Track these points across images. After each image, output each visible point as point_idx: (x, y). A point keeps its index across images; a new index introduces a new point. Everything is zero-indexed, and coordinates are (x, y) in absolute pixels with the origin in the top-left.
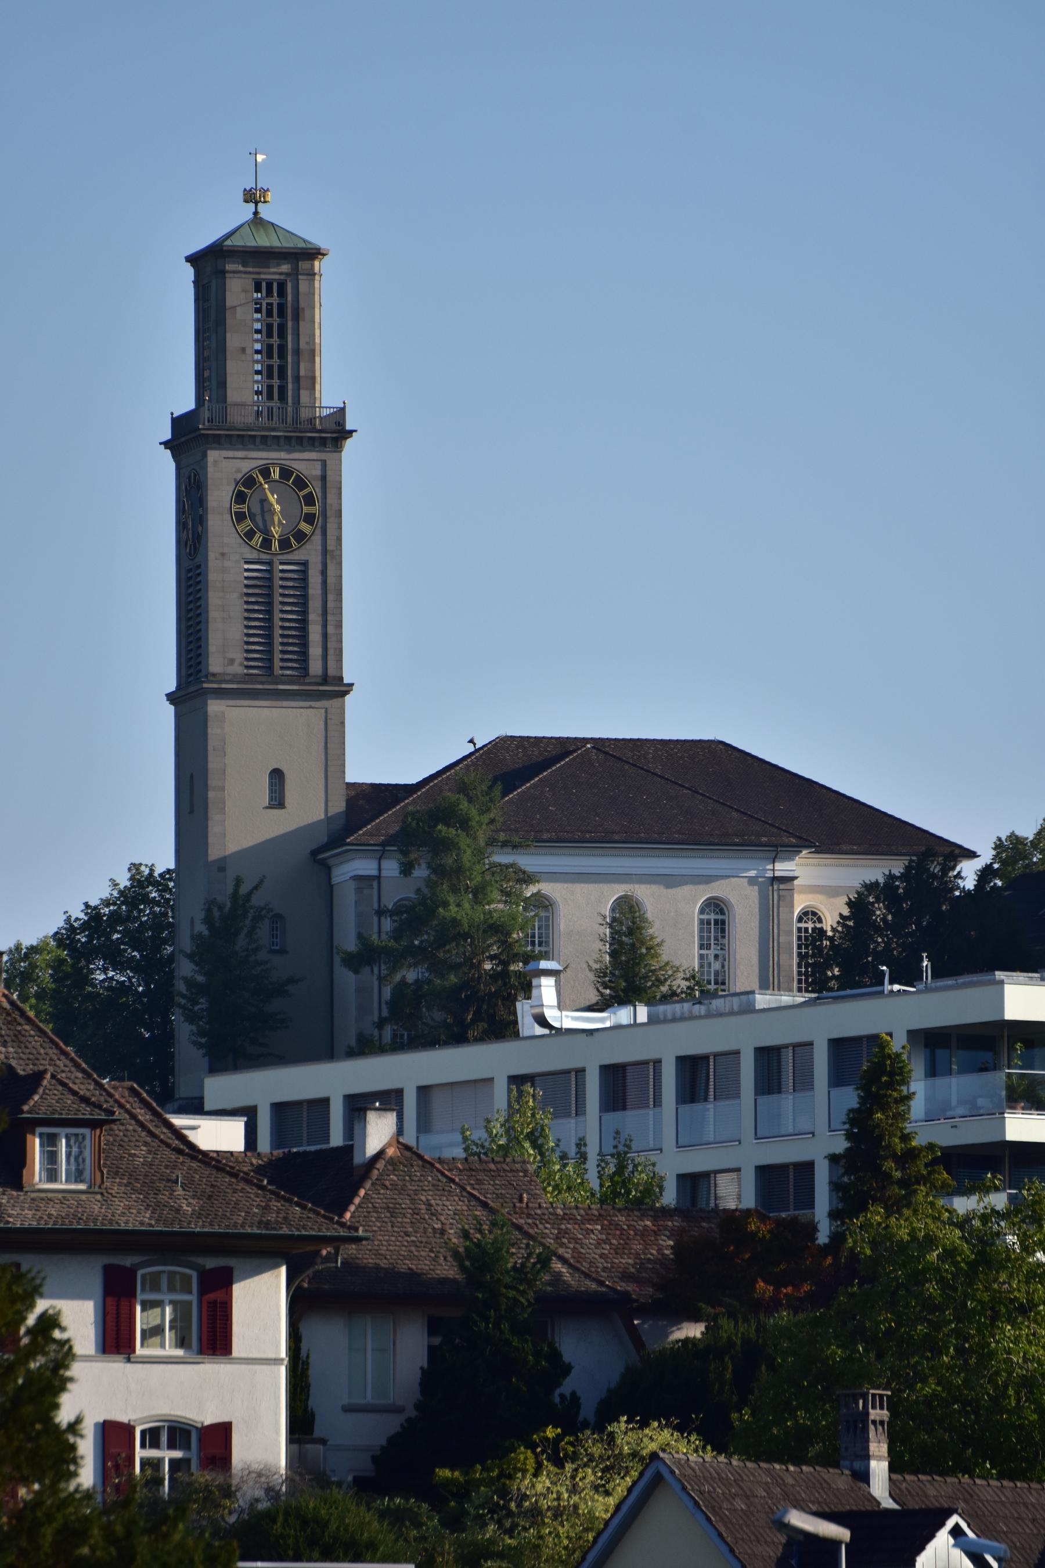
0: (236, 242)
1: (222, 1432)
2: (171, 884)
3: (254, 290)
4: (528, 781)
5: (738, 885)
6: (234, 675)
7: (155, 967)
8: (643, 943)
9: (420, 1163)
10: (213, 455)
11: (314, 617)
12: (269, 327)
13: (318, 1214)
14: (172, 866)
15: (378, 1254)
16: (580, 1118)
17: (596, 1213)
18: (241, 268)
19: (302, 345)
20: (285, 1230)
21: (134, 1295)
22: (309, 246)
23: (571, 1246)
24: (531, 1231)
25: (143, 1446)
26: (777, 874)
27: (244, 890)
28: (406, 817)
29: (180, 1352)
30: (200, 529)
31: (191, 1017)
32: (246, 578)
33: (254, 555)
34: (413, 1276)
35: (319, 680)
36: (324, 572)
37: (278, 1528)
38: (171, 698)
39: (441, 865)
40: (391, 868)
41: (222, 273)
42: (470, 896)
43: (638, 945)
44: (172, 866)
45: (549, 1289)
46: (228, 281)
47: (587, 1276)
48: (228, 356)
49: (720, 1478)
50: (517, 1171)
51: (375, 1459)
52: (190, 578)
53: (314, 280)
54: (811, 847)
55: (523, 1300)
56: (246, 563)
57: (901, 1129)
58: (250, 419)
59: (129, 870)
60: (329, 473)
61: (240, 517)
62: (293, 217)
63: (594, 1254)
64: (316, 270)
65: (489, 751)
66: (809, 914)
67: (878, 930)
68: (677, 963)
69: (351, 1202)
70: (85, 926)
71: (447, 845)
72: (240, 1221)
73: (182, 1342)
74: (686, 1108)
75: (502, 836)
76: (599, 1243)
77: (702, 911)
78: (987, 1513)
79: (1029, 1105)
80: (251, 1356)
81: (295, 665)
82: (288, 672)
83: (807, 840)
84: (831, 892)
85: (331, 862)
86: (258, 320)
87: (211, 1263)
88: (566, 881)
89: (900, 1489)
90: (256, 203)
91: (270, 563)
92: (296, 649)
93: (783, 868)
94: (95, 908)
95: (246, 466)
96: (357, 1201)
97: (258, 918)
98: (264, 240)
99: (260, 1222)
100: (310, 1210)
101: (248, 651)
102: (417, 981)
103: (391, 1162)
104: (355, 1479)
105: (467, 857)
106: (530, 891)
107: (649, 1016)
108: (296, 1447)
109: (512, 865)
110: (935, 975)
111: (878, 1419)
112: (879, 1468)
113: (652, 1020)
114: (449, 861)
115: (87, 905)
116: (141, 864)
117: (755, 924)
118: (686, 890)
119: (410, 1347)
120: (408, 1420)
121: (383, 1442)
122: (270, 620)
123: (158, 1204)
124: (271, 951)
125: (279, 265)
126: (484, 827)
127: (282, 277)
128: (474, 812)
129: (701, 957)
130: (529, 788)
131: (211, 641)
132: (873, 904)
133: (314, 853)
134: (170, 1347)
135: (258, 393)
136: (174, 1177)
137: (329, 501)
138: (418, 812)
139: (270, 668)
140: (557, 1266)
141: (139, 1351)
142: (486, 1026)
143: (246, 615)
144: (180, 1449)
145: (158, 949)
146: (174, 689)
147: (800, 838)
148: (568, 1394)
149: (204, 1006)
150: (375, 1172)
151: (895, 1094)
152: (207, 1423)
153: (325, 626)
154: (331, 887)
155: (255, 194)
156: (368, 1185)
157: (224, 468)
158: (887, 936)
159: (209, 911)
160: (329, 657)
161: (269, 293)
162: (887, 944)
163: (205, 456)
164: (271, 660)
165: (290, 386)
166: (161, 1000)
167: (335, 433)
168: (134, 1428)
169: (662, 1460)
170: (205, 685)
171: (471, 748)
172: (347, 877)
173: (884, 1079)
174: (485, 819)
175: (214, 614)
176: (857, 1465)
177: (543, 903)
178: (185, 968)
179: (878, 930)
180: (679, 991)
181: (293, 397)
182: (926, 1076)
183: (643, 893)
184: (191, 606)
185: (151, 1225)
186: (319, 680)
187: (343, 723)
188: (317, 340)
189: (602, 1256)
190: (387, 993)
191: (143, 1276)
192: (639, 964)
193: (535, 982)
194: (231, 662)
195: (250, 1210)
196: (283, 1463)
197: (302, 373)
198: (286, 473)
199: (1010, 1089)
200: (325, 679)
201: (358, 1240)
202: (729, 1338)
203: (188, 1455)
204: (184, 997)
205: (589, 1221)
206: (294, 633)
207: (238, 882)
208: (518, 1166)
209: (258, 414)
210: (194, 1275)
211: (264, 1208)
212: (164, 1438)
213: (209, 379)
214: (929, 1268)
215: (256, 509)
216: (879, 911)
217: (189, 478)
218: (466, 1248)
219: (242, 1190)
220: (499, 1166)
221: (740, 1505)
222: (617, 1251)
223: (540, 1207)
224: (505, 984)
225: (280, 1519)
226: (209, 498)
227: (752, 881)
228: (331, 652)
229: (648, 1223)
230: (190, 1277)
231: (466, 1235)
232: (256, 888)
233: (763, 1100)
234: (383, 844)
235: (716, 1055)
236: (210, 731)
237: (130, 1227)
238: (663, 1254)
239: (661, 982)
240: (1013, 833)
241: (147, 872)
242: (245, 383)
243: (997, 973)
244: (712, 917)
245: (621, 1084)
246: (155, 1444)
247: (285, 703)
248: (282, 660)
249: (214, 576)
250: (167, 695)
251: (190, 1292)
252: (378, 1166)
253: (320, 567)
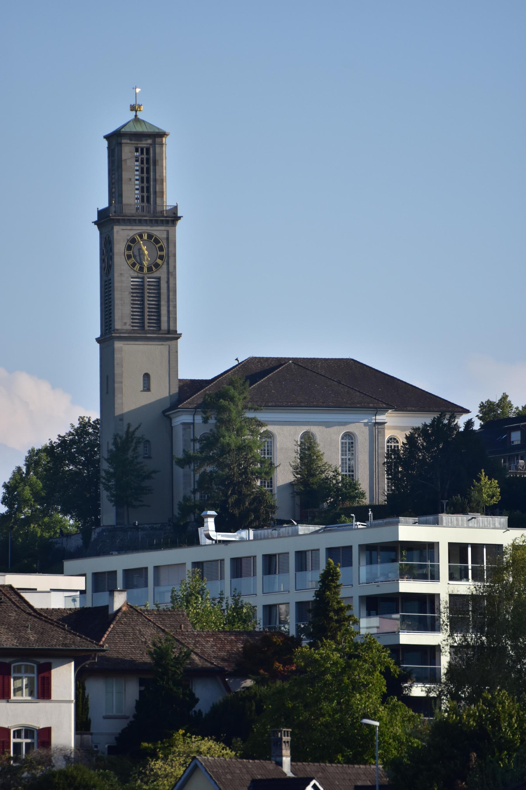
0: (126, 129)
1: (47, 732)
2: (99, 426)
3: (136, 152)
4: (262, 379)
5: (359, 426)
6: (127, 330)
7: (92, 462)
8: (314, 454)
9: (137, 613)
10: (116, 228)
11: (163, 303)
12: (142, 169)
13: (87, 640)
14: (99, 417)
15: (118, 652)
16: (222, 581)
17: (211, 633)
18: (129, 141)
19: (158, 177)
20: (73, 647)
21: (10, 675)
22: (160, 131)
23: (200, 648)
24: (183, 642)
25: (14, 737)
26: (377, 421)
27: (131, 429)
28: (205, 396)
29: (29, 698)
30: (111, 262)
31: (108, 489)
32: (132, 285)
33: (135, 274)
34: (132, 662)
35: (166, 332)
36: (168, 282)
37: (56, 780)
38: (98, 340)
39: (221, 418)
40: (199, 419)
41: (120, 144)
42: (235, 432)
43: (312, 455)
44: (99, 417)
45: (190, 666)
46: (123, 148)
47: (206, 660)
48: (123, 182)
49: (221, 766)
50: (180, 615)
51: (116, 739)
52: (106, 285)
53: (163, 147)
54: (393, 409)
55: (178, 672)
56: (132, 278)
57: (337, 598)
58: (134, 212)
59: (79, 420)
60: (170, 236)
61: (129, 257)
62: (153, 118)
63: (210, 651)
64: (164, 142)
65: (245, 364)
66: (392, 439)
67: (420, 450)
68: (330, 463)
69: (107, 630)
70: (59, 445)
71: (222, 409)
72: (54, 643)
73: (31, 694)
74: (267, 577)
75: (249, 405)
76: (212, 646)
77: (342, 438)
78: (331, 777)
79: (409, 577)
80: (61, 699)
81: (154, 325)
82: (152, 328)
83: (391, 405)
84: (402, 429)
85: (172, 416)
86: (137, 166)
87: (42, 661)
88: (279, 425)
89: (295, 768)
90: (136, 111)
91: (143, 278)
92: (155, 318)
93: (380, 418)
94: (64, 437)
95: (132, 233)
96: (110, 630)
97: (138, 442)
98: (139, 129)
99: (63, 644)
100: (84, 638)
101: (133, 319)
102: (211, 471)
103: (125, 613)
104: (109, 747)
105: (234, 415)
106: (262, 430)
107: (254, 536)
108: (79, 736)
109: (254, 418)
110: (374, 519)
111: (286, 740)
112: (286, 760)
113: (256, 538)
114: (225, 416)
115: (59, 436)
116: (84, 417)
117: (367, 444)
118: (335, 429)
119: (131, 691)
120: (131, 722)
121: (120, 731)
122: (143, 304)
123: (20, 636)
124: (144, 458)
125: (146, 140)
126: (241, 400)
127: (148, 146)
128: (236, 394)
129: (342, 459)
130: (263, 382)
131: (116, 314)
132: (417, 438)
133: (164, 412)
134: (26, 696)
135: (137, 199)
136: (27, 625)
137: (170, 249)
138: (211, 394)
139: (143, 327)
140: (194, 657)
141: (12, 697)
142: (237, 496)
143: (132, 302)
144: (30, 738)
145: (93, 456)
146: (99, 336)
147: (388, 404)
148: (197, 710)
149: (113, 483)
150: (117, 618)
151: (334, 584)
152: (41, 727)
153: (168, 307)
154: (172, 427)
155: (135, 107)
156: (114, 623)
157: (122, 234)
158: (423, 452)
159: (115, 439)
160: (170, 321)
161: (142, 153)
162: (423, 456)
163: (113, 228)
164: (143, 323)
165: (152, 196)
166: (93, 481)
167: (173, 218)
168: (10, 730)
169: (197, 759)
170: (113, 335)
171: (236, 363)
172: (179, 423)
173: (330, 578)
174: (242, 397)
175: (117, 302)
176: (278, 759)
177: (269, 435)
178: (105, 465)
179: (420, 450)
180: (329, 477)
181: (153, 201)
182: (367, 564)
183: (315, 430)
184: (107, 298)
185: (17, 646)
186: (166, 332)
187: (177, 352)
188: (164, 174)
189: (213, 652)
190: (197, 476)
191: (14, 667)
192: (312, 463)
193: (205, 520)
194: (125, 324)
195: (58, 638)
196: (73, 745)
197: (157, 190)
198: (150, 236)
199: (401, 570)
200: (169, 332)
201: (104, 651)
202: (255, 693)
203: (33, 741)
204: (104, 478)
205: (208, 637)
206: (154, 310)
207: (129, 426)
208: (180, 613)
209: (137, 209)
210: (35, 666)
211: (65, 638)
212: (23, 734)
213: (115, 192)
214: (327, 669)
215: (137, 253)
216: (420, 441)
217: (106, 239)
218: (155, 650)
219: (56, 630)
220: (172, 613)
221: (229, 777)
222: (220, 649)
223: (187, 631)
224: (246, 477)
225: (57, 776)
226: (115, 248)
227: (366, 424)
228: (171, 319)
229: (233, 638)
230: (34, 667)
231: (154, 644)
232: (137, 428)
233: (299, 574)
234: (196, 408)
235: (279, 554)
236: (115, 356)
237: (8, 647)
238: (239, 651)
239: (323, 472)
240: (488, 400)
241: (87, 420)
242: (131, 195)
243: (400, 518)
244: (347, 441)
245: (239, 567)
246: (19, 737)
247: (150, 343)
248: (149, 323)
249: (117, 284)
250: (96, 339)
251: (34, 673)
252: (119, 615)
253: (166, 280)
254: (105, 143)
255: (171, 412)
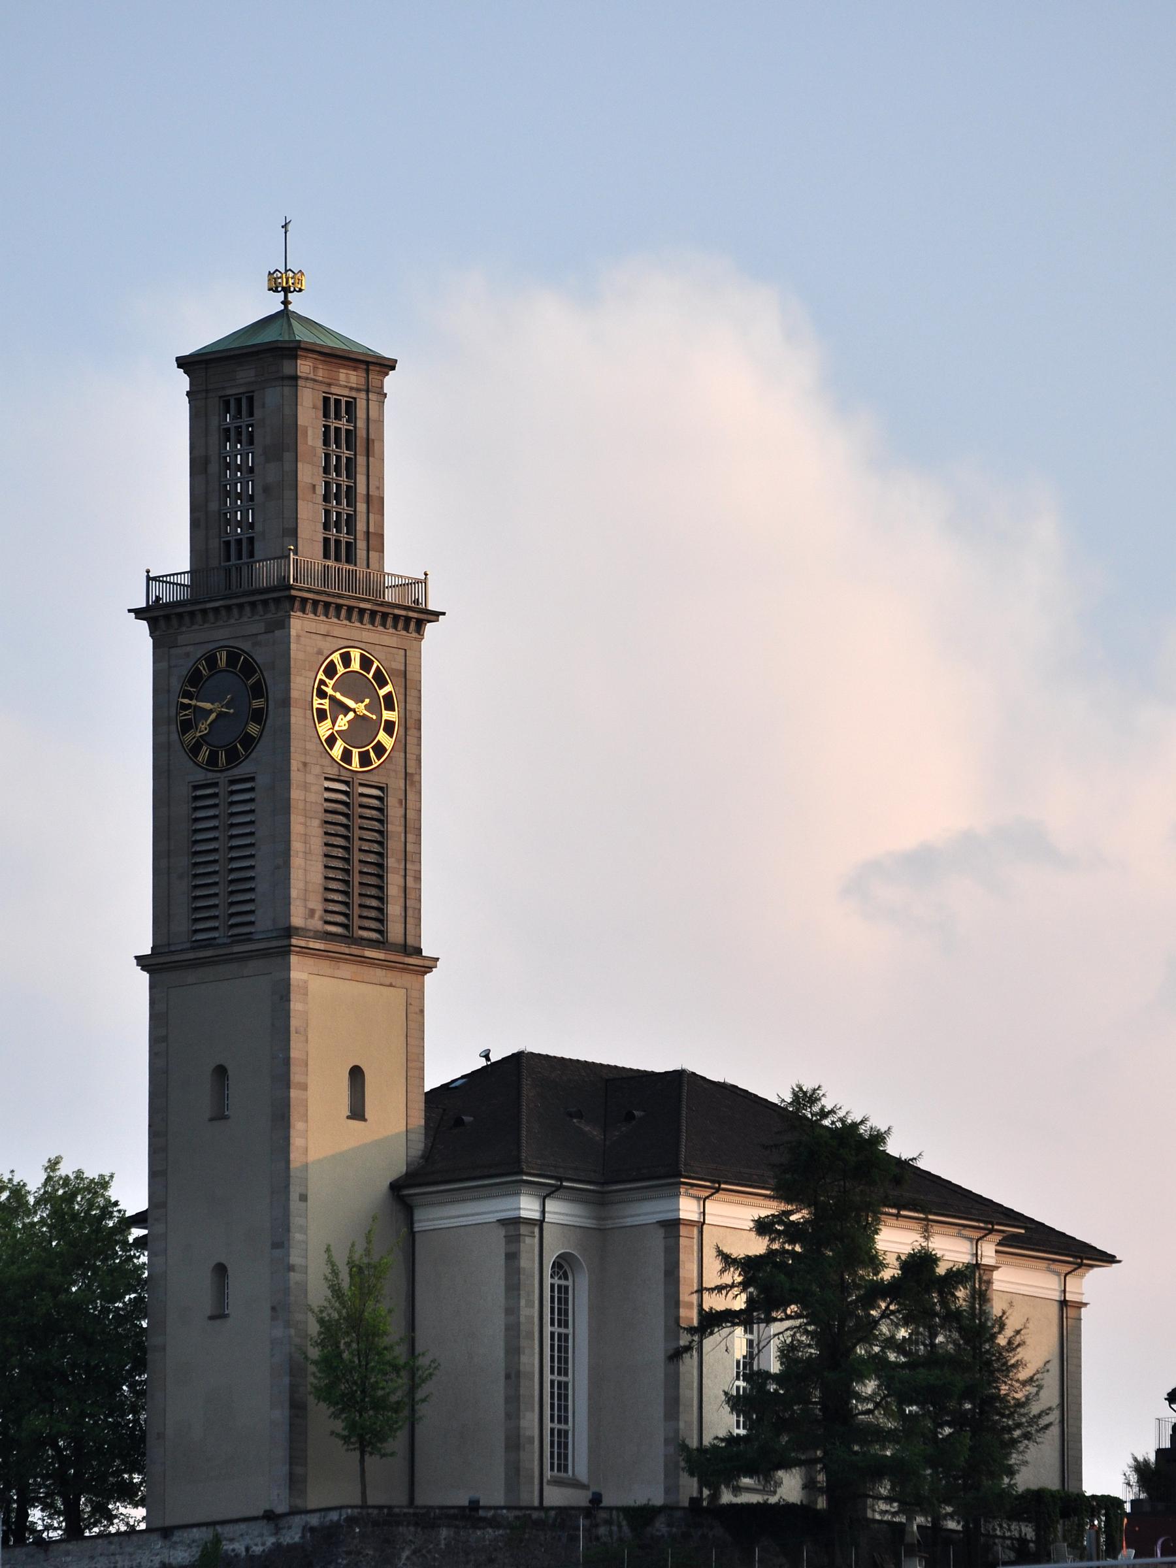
3: (274, 415)
6: (316, 932)
32: (326, 800)
33: (333, 771)
90: (286, 290)
154: (412, 1233)
167: (414, 618)
171: (483, 1063)
187: (422, 1011)
228: (410, 913)
254: (183, 381)
255: (412, 1191)
